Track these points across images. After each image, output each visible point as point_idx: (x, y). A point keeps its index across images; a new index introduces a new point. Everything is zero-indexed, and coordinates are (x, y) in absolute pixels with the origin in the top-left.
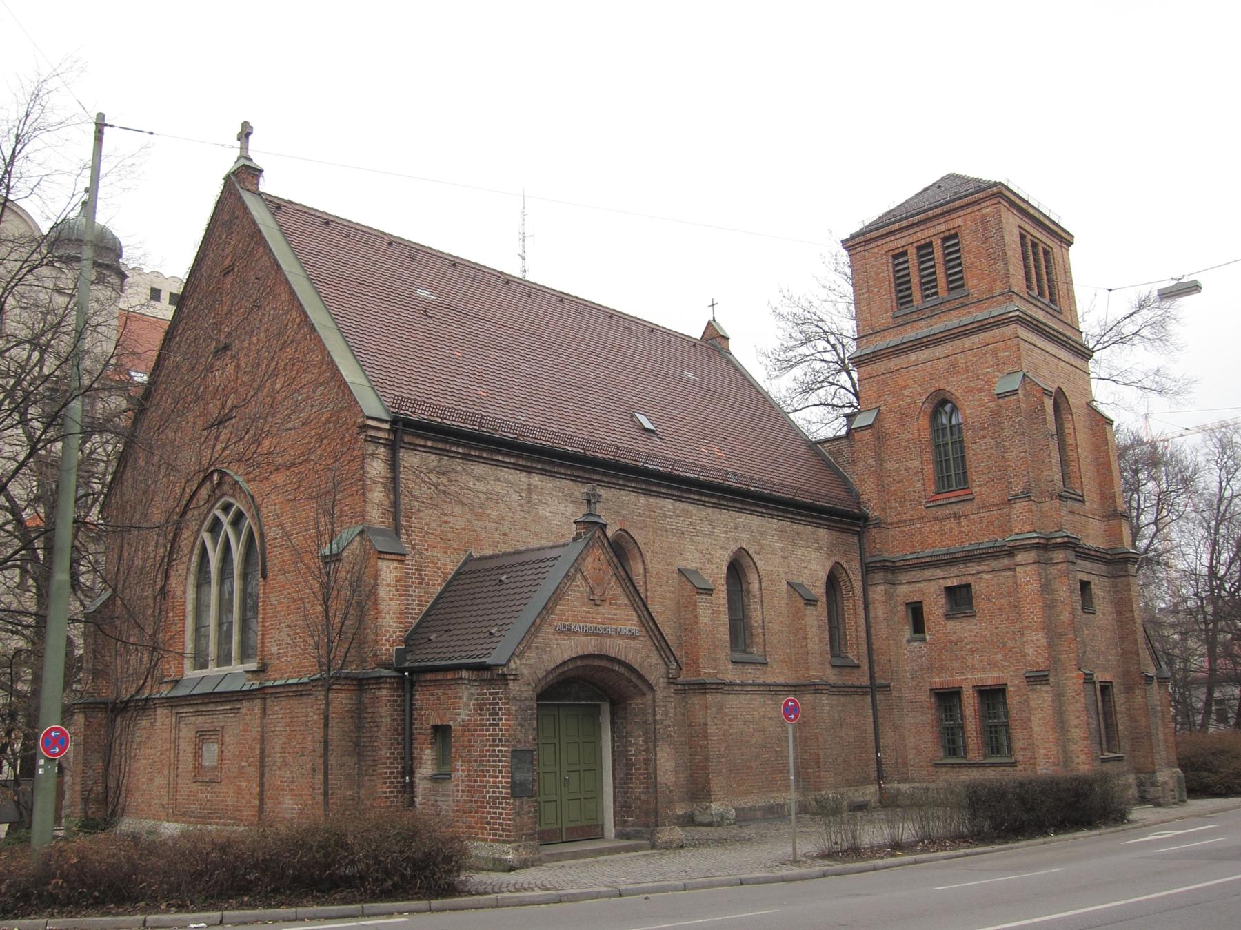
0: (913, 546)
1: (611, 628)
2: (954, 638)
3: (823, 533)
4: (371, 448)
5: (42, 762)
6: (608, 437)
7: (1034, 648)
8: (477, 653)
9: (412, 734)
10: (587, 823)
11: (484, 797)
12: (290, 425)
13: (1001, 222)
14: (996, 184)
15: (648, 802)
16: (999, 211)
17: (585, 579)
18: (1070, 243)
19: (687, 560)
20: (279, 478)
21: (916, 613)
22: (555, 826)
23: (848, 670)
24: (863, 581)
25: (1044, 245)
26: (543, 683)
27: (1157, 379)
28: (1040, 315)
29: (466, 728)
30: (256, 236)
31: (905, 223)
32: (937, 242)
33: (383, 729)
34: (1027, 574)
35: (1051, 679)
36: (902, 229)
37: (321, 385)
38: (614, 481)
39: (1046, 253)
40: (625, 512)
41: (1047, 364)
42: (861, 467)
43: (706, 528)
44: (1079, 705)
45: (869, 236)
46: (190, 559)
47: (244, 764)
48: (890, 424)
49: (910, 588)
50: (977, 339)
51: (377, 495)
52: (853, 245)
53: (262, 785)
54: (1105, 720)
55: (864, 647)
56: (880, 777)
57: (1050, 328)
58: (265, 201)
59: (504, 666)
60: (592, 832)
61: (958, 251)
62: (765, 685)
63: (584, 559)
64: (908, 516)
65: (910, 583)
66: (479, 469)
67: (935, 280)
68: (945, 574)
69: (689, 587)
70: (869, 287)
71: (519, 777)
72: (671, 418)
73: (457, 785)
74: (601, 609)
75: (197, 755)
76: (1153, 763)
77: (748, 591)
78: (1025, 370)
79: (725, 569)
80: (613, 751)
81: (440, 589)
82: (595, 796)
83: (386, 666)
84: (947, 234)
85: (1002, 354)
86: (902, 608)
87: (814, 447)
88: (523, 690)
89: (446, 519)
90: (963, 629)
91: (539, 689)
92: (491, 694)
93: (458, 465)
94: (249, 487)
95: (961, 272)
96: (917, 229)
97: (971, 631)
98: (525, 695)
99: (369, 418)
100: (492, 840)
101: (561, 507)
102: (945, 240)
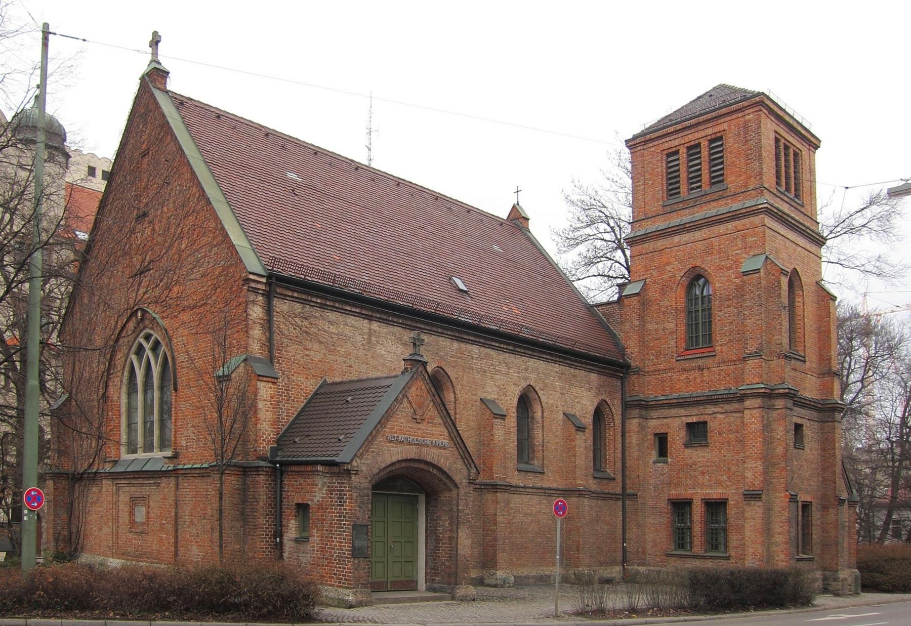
0: (664, 390)
1: (428, 440)
2: (690, 462)
3: (593, 376)
4: (252, 297)
6: (432, 295)
7: (753, 473)
9: (281, 508)
11: (332, 556)
12: (192, 277)
13: (760, 127)
15: (450, 567)
16: (759, 118)
17: (410, 403)
20: (185, 317)
21: (662, 442)
23: (605, 481)
26: (377, 478)
28: (785, 208)
29: (320, 506)
33: (261, 504)
35: (764, 497)
37: (215, 246)
39: (796, 155)
40: (442, 354)
41: (787, 248)
42: (627, 326)
43: (504, 369)
44: (783, 518)
45: (648, 137)
50: (730, 226)
51: (257, 332)
52: (636, 144)
53: (176, 537)
54: (803, 530)
55: (619, 465)
56: (624, 561)
62: (541, 488)
63: (409, 388)
66: (332, 316)
68: (687, 413)
71: (358, 543)
74: (421, 426)
75: (131, 513)
76: (837, 564)
77: (533, 418)
78: (768, 253)
79: (516, 401)
81: (302, 405)
82: (413, 561)
83: (263, 459)
84: (713, 136)
87: (591, 308)
89: (307, 352)
90: (698, 455)
91: (373, 482)
92: (339, 483)
93: (317, 312)
98: (363, 485)
99: (250, 273)
100: (338, 586)
101: (394, 348)
102: (711, 141)
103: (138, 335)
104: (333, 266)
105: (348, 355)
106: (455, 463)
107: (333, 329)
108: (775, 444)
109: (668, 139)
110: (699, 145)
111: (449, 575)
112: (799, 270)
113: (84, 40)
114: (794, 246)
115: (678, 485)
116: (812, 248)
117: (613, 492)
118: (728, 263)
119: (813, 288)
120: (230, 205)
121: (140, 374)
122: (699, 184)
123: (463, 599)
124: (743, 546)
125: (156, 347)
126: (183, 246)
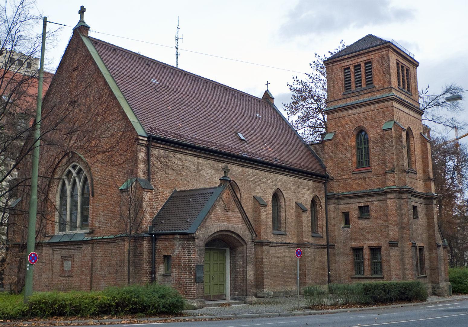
0: (346, 189)
2: (361, 227)
3: (310, 183)
4: (139, 147)
5: (28, 265)
6: (229, 144)
7: (393, 232)
8: (182, 228)
9: (155, 258)
10: (220, 294)
11: (185, 282)
12: (104, 136)
13: (389, 58)
14: (388, 42)
15: (243, 286)
16: (388, 53)
17: (223, 201)
18: (417, 66)
19: (257, 193)
20: (99, 157)
21: (346, 216)
22: (208, 294)
23: (318, 238)
24: (325, 203)
25: (408, 65)
26: (207, 240)
27: (452, 122)
28: (403, 97)
29: (178, 256)
30: (88, 56)
31: (350, 56)
32: (362, 64)
33: (144, 256)
34: (392, 202)
35: (399, 245)
36: (349, 58)
37: (119, 121)
38: (230, 161)
39: (407, 70)
40: (234, 173)
41: (405, 117)
42: (326, 156)
43: (265, 181)
44: (409, 255)
45: (334, 60)
46: (58, 187)
47: (84, 269)
48: (340, 139)
49: (345, 206)
50: (376, 106)
51: (142, 166)
52: (330, 63)
53: (92, 277)
54: (420, 262)
55: (325, 229)
56: (329, 281)
57: (407, 102)
58: (90, 39)
59: (194, 233)
60: (220, 297)
61: (371, 69)
62: (285, 243)
63: (223, 194)
64: (345, 177)
65: (345, 204)
66: (179, 156)
67: (361, 80)
68: (358, 201)
69: (258, 204)
70: (333, 81)
71: (198, 275)
72: (251, 134)
73: (174, 278)
74: (228, 213)
75: (62, 265)
76: (438, 279)
77: (280, 206)
78: (395, 120)
79: (271, 197)
80: (230, 267)
81: (164, 203)
82: (223, 284)
83: (146, 232)
84: (367, 61)
85: (386, 113)
86: (341, 214)
87: (307, 146)
88: (200, 243)
90: (365, 224)
91: (205, 243)
92: (188, 244)
94: (87, 160)
95: (371, 77)
96: (354, 59)
97: (368, 224)
98: (201, 245)
99: (140, 136)
100: (188, 298)
101: (210, 171)
102: (366, 64)
103: (68, 166)
104: (179, 129)
105: (187, 176)
106: (245, 231)
107: (179, 163)
108: (403, 217)
109: (344, 61)
110: (360, 65)
111: (243, 290)
112: (411, 128)
113: (65, 25)
114: (408, 116)
115: (355, 240)
116: (417, 116)
117: (322, 244)
118: (377, 125)
119: (419, 136)
120: (126, 99)
121: (68, 188)
122: (360, 84)
123: (250, 303)
124: (390, 271)
125: (79, 172)
126: (99, 120)
